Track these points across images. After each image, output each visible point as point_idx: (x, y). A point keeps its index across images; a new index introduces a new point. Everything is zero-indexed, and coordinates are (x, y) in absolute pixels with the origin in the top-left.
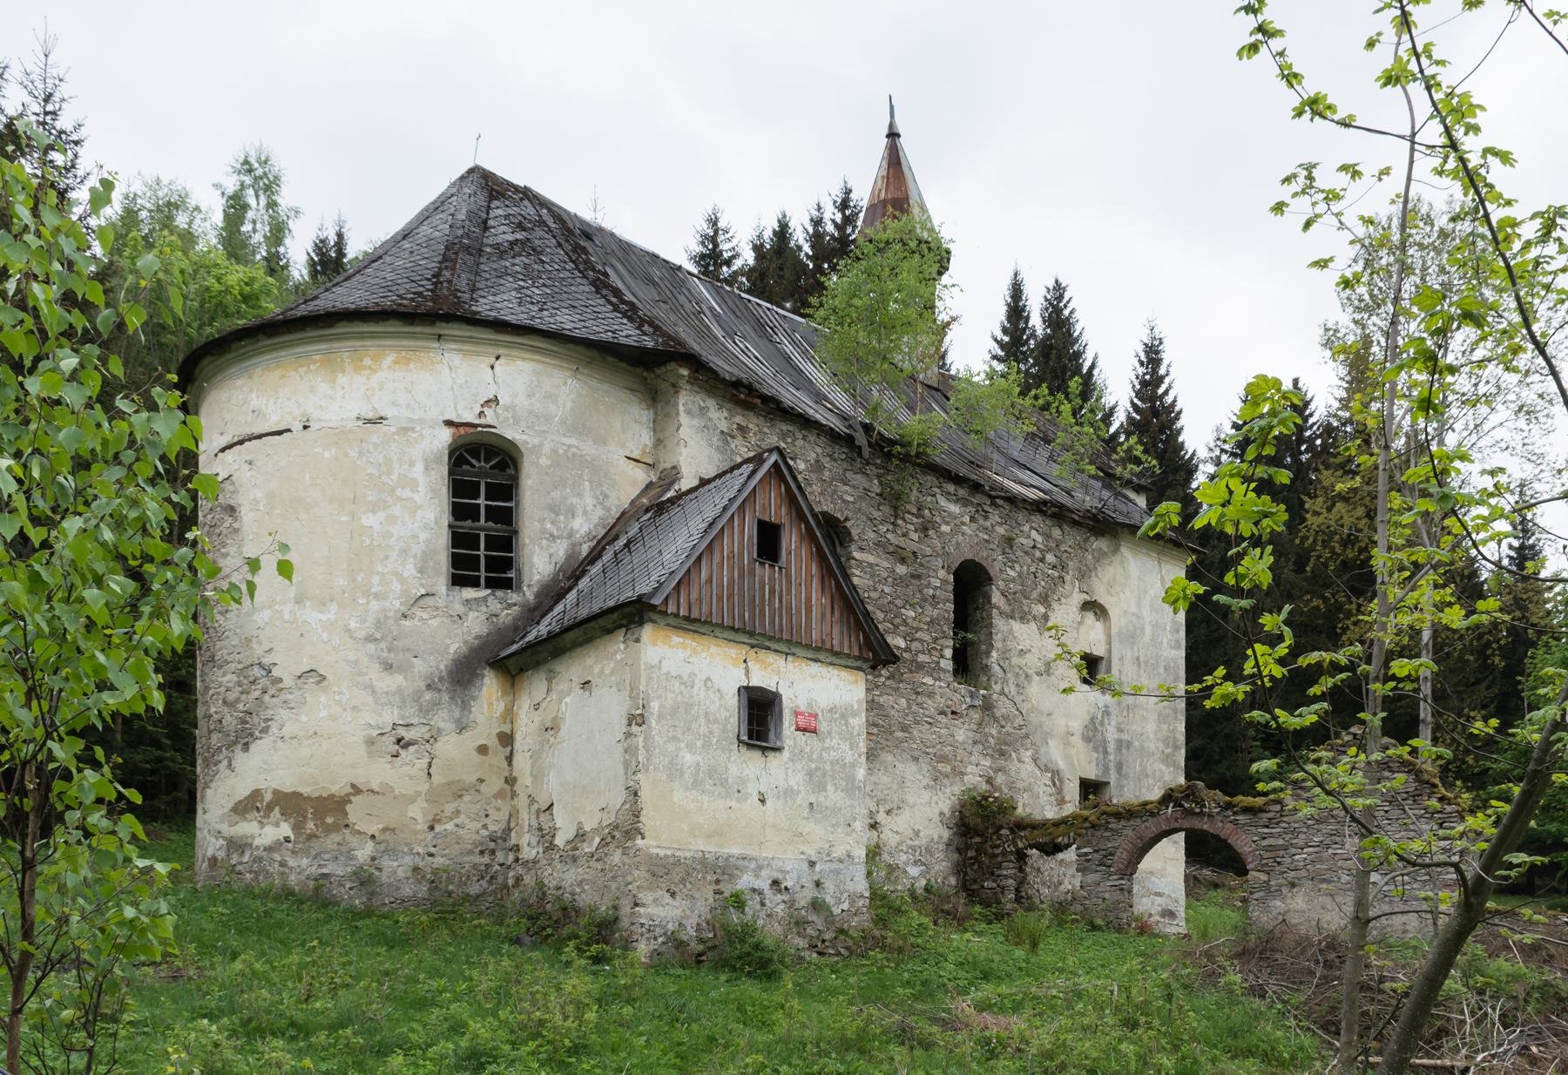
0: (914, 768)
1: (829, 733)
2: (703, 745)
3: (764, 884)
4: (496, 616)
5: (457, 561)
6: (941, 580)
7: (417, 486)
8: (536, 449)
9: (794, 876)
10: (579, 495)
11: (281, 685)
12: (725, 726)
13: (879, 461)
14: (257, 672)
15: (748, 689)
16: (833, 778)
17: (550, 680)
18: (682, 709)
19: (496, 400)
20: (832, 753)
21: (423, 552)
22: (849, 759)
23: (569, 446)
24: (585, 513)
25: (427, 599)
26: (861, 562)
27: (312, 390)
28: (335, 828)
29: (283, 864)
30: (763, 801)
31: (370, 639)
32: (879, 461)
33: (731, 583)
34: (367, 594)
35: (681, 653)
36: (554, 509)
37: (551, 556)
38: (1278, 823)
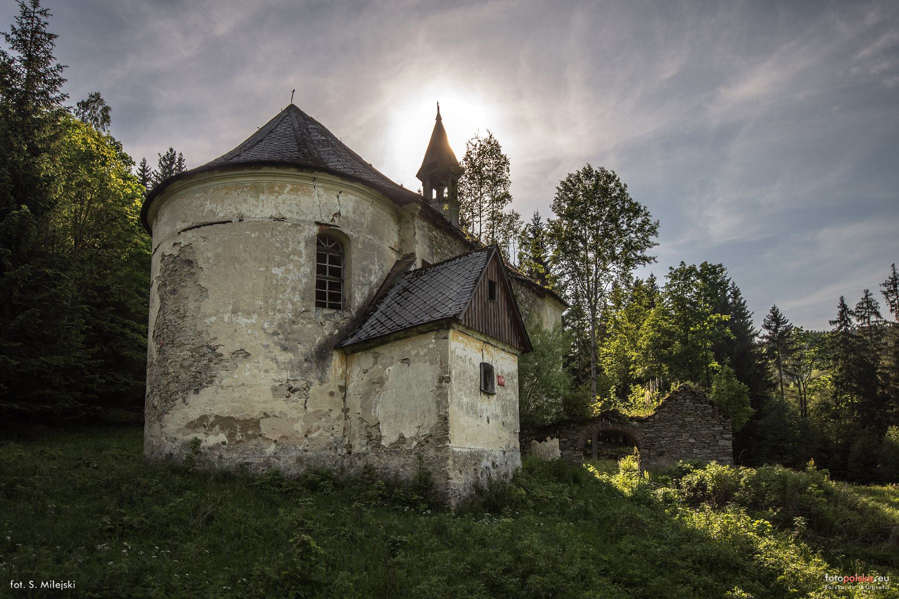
4: (338, 323)
5: (320, 296)
7: (302, 254)
8: (357, 239)
10: (373, 264)
11: (222, 358)
14: (205, 350)
15: (483, 363)
17: (376, 358)
21: (304, 289)
23: (370, 239)
24: (375, 273)
25: (305, 313)
27: (245, 201)
28: (254, 437)
29: (221, 457)
31: (275, 333)
34: (274, 309)
35: (462, 345)
36: (364, 270)
37: (362, 293)
38: (652, 427)
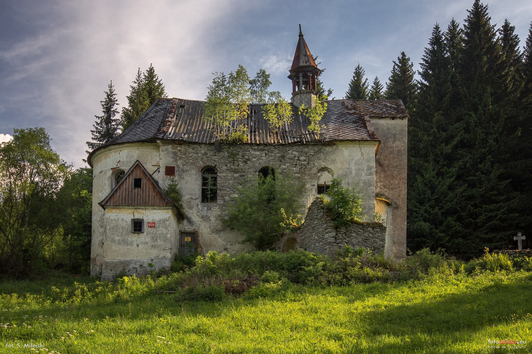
2: (121, 235)
3: (137, 266)
12: (127, 229)
13: (226, 147)
16: (160, 238)
20: (160, 232)
22: (165, 232)
26: (221, 176)
30: (138, 246)
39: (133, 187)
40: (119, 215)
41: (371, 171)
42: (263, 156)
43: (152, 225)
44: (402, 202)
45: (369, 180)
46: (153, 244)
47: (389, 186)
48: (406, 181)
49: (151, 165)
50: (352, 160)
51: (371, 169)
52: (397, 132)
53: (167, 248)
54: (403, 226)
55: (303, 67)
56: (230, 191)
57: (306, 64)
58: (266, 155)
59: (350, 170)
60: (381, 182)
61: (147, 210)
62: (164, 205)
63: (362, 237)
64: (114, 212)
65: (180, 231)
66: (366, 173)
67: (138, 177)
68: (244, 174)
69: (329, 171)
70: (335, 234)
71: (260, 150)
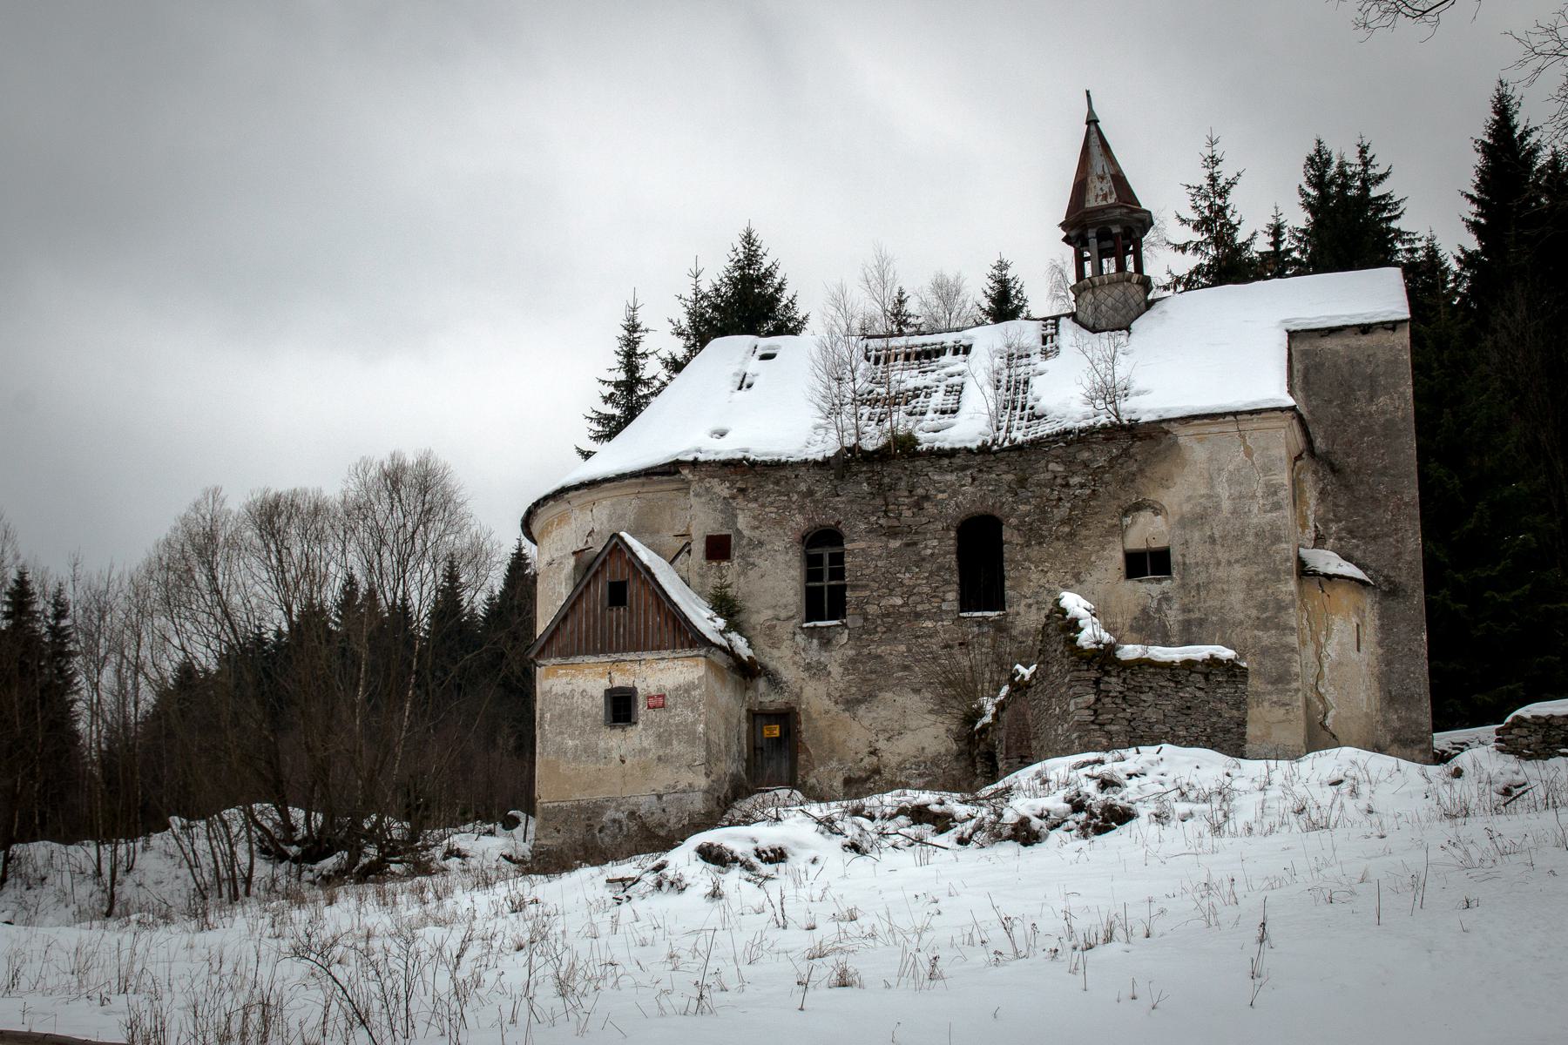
0: (917, 698)
1: (675, 705)
6: (940, 546)
9: (647, 807)
13: (865, 469)
16: (677, 735)
18: (566, 714)
19: (593, 531)
32: (865, 469)
33: (587, 631)
39: (606, 603)
40: (574, 681)
41: (1275, 498)
42: (965, 485)
43: (659, 702)
44: (1408, 573)
45: (1272, 524)
46: (661, 753)
47: (1364, 531)
48: (1417, 512)
49: (671, 534)
50: (1220, 470)
51: (1275, 493)
52: (1381, 369)
53: (697, 763)
54: (1415, 646)
55: (1099, 210)
56: (879, 588)
57: (1104, 203)
58: (974, 479)
59: (1215, 500)
60: (1341, 521)
61: (643, 663)
62: (686, 644)
63: (1174, 702)
64: (561, 676)
65: (748, 710)
66: (1264, 505)
67: (619, 578)
68: (916, 538)
69: (1156, 509)
70: (1092, 698)
71: (956, 469)
